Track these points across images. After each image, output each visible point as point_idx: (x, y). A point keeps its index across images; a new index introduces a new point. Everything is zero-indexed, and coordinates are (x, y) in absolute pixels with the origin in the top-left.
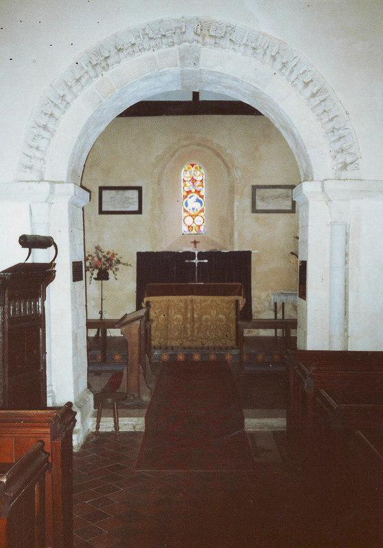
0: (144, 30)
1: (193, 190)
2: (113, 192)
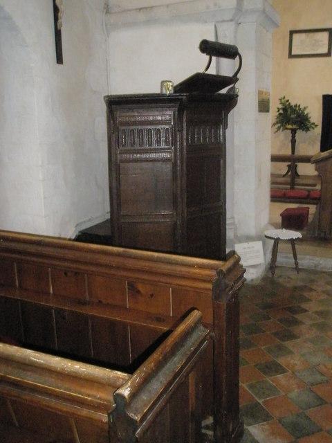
2: (303, 36)
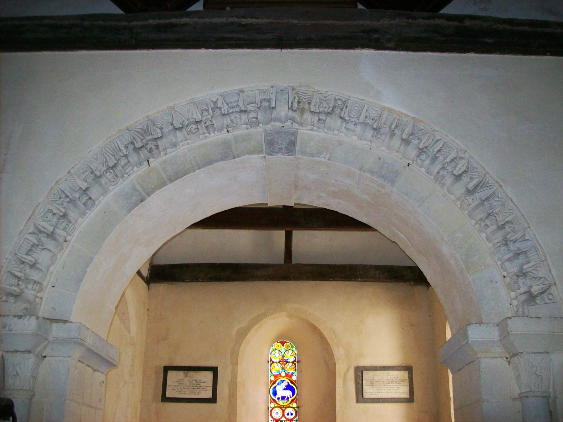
0: (215, 103)
1: (283, 374)
2: (181, 374)
